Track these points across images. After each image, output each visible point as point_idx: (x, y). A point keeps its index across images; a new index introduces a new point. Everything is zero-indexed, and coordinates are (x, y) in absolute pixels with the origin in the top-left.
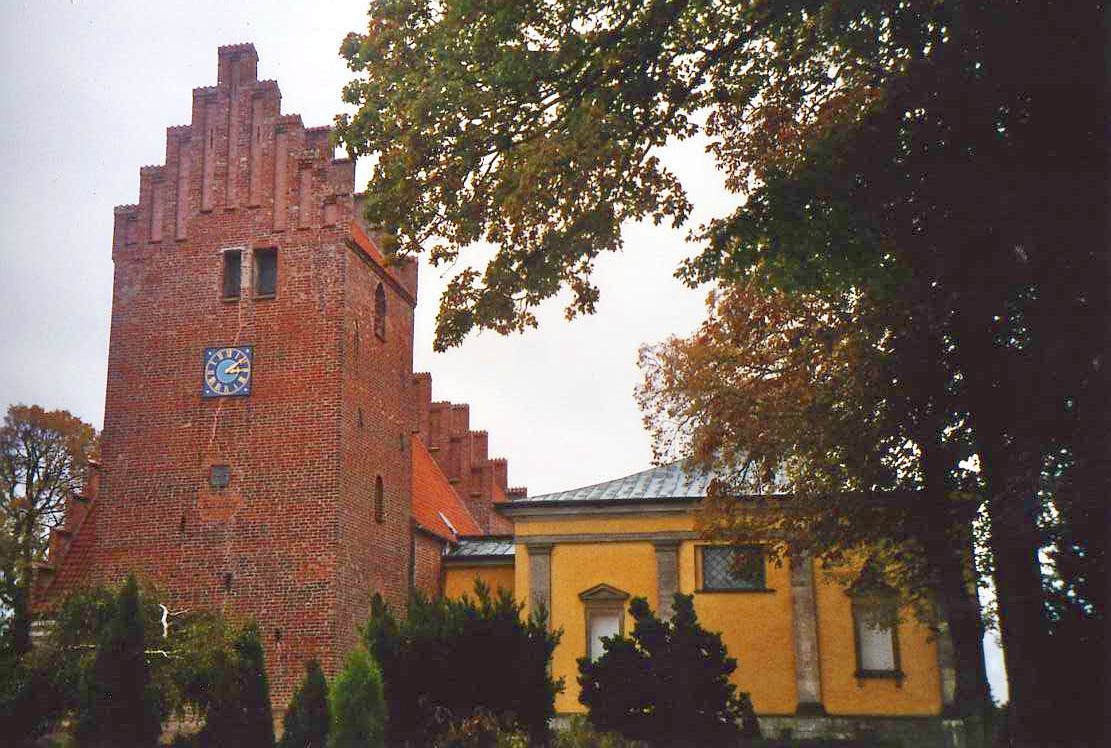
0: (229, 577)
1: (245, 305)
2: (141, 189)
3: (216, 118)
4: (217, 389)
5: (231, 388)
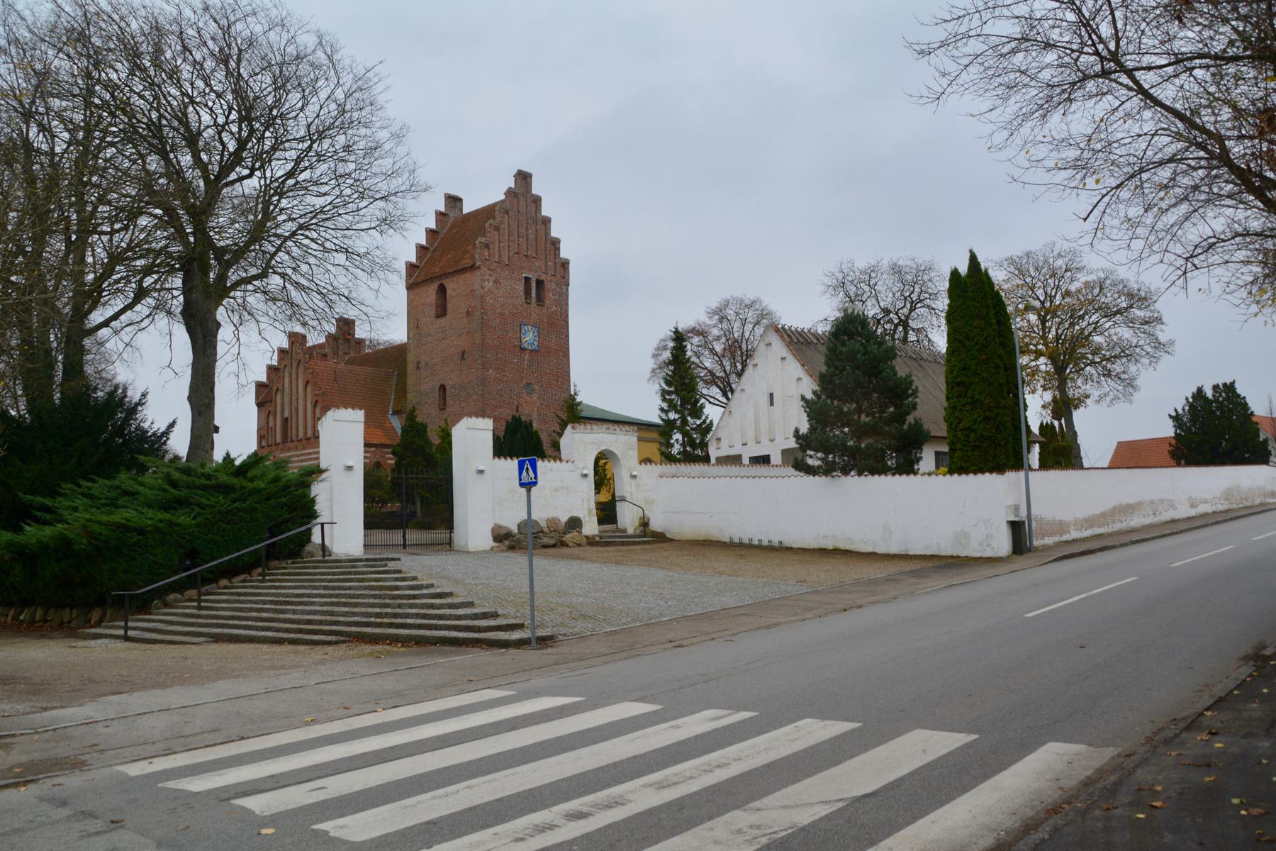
4: (526, 345)
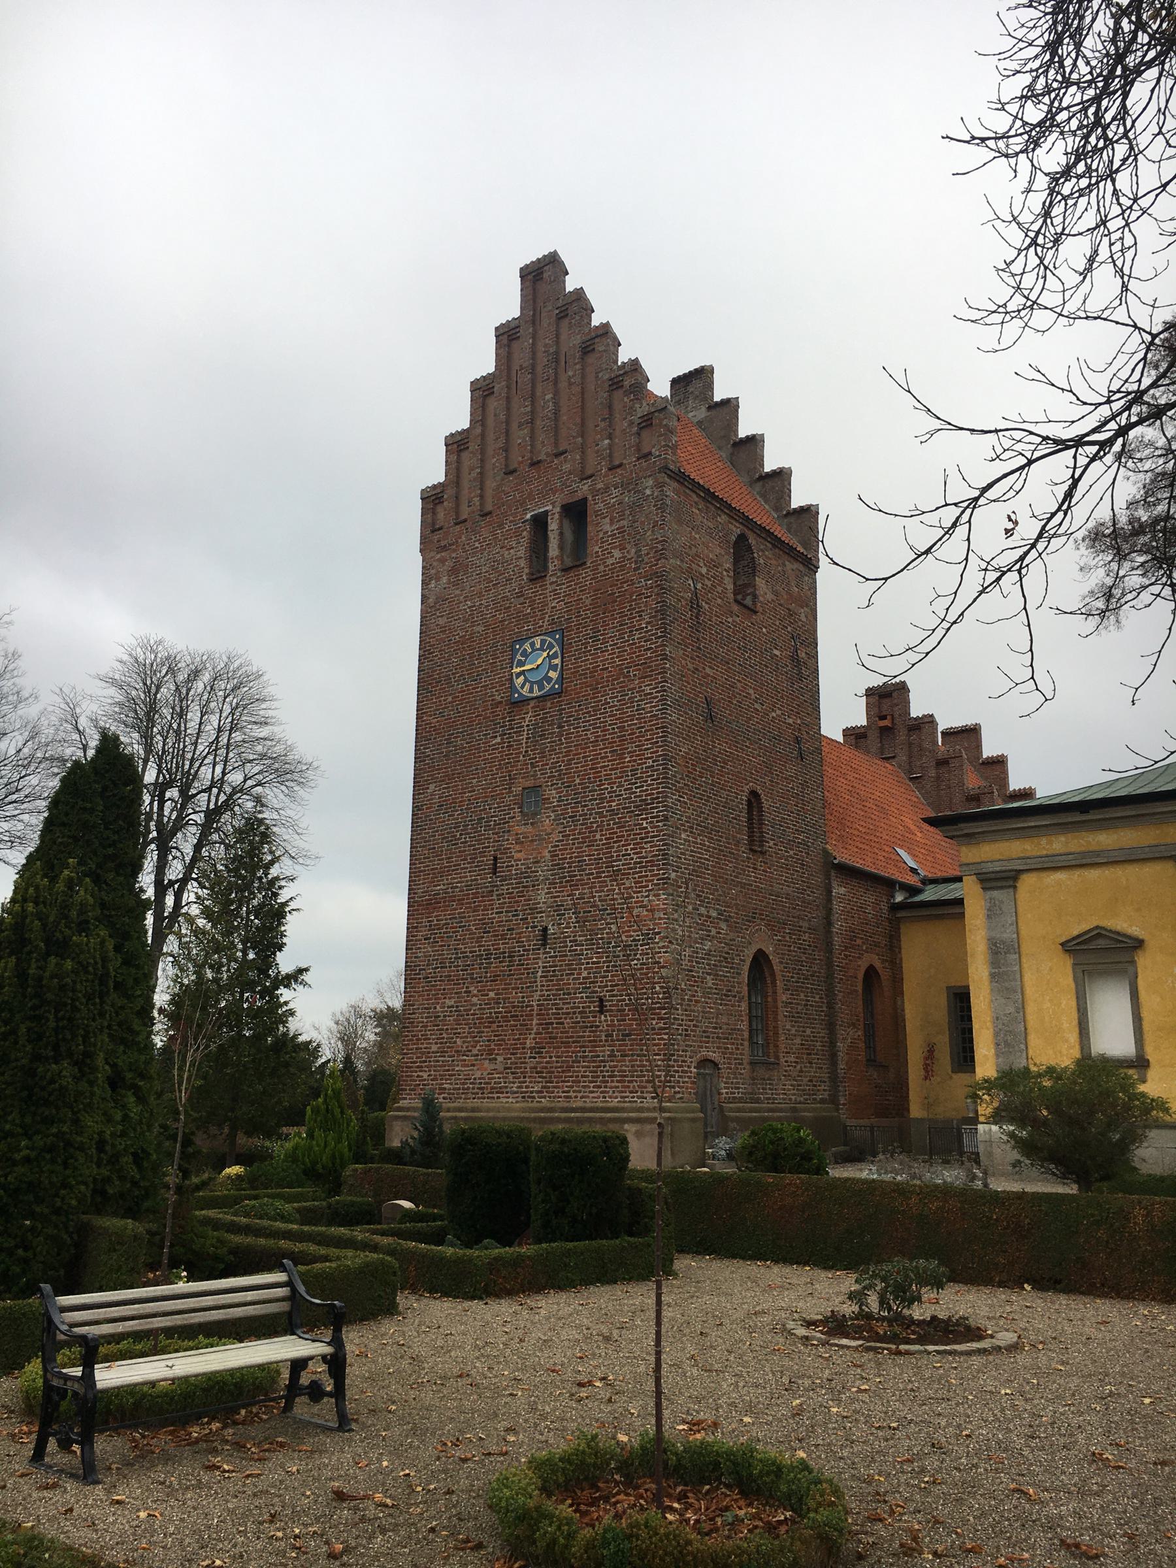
0: (545, 929)
2: (446, 462)
4: (525, 691)
5: (541, 688)
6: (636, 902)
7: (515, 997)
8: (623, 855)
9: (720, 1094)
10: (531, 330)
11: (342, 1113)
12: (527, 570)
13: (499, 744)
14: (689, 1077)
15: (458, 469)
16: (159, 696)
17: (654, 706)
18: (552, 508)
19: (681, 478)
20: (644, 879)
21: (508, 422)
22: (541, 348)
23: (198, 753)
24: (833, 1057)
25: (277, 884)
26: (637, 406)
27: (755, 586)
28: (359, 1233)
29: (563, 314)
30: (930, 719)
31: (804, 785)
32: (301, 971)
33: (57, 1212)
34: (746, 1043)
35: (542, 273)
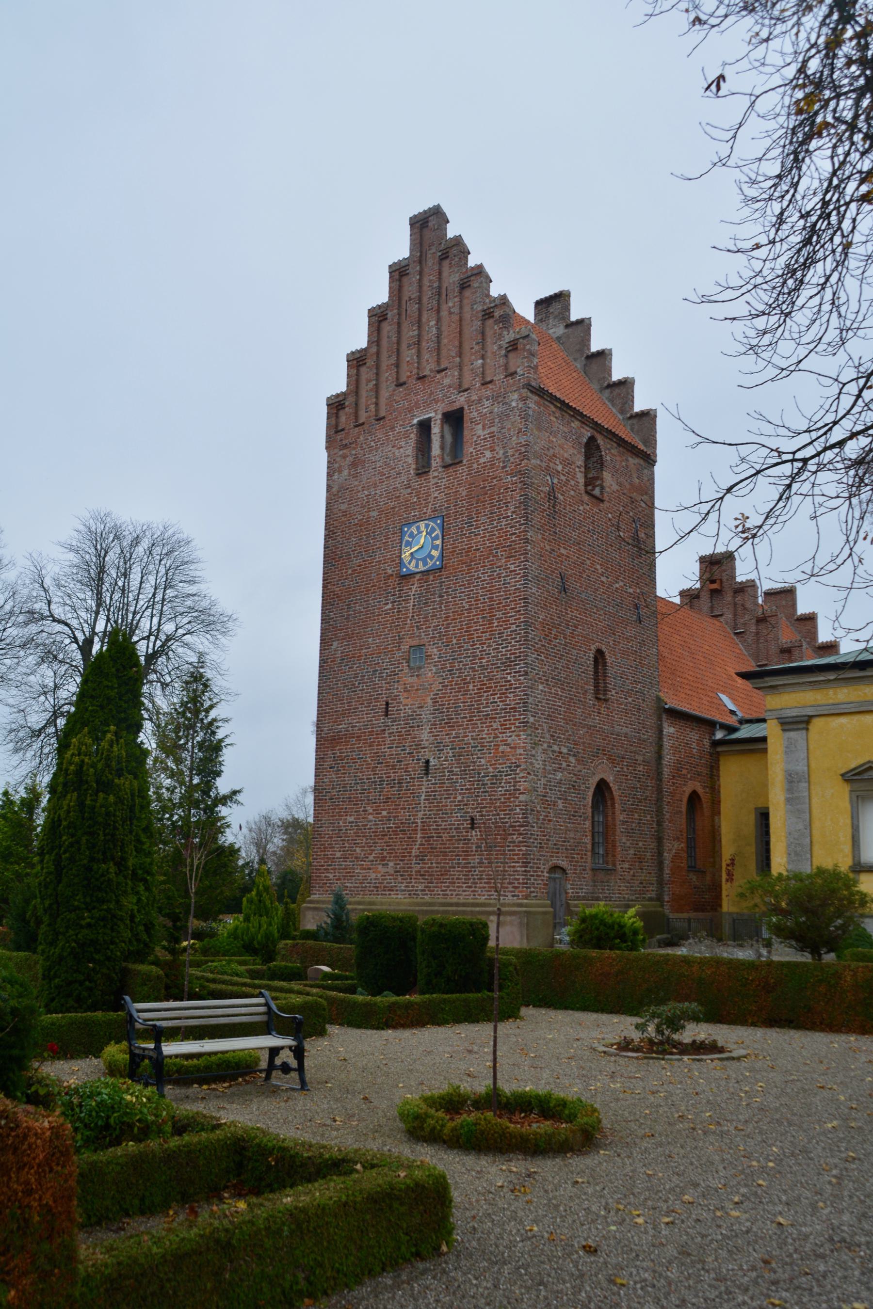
0: (427, 762)
1: (436, 474)
2: (348, 375)
3: (410, 289)
4: (412, 567)
5: (425, 564)
6: (501, 741)
7: (403, 815)
8: (492, 703)
9: (567, 893)
10: (418, 268)
11: (272, 903)
12: (414, 466)
13: (390, 609)
14: (542, 880)
15: (357, 381)
16: (107, 559)
17: (518, 581)
18: (435, 415)
19: (541, 392)
20: (508, 722)
21: (399, 343)
22: (426, 282)
23: (139, 606)
24: (661, 864)
25: (216, 724)
26: (505, 333)
27: (602, 479)
28: (295, 985)
29: (444, 256)
30: (752, 584)
31: (642, 643)
32: (235, 793)
33: (108, 959)
34: (589, 854)
35: (427, 222)
